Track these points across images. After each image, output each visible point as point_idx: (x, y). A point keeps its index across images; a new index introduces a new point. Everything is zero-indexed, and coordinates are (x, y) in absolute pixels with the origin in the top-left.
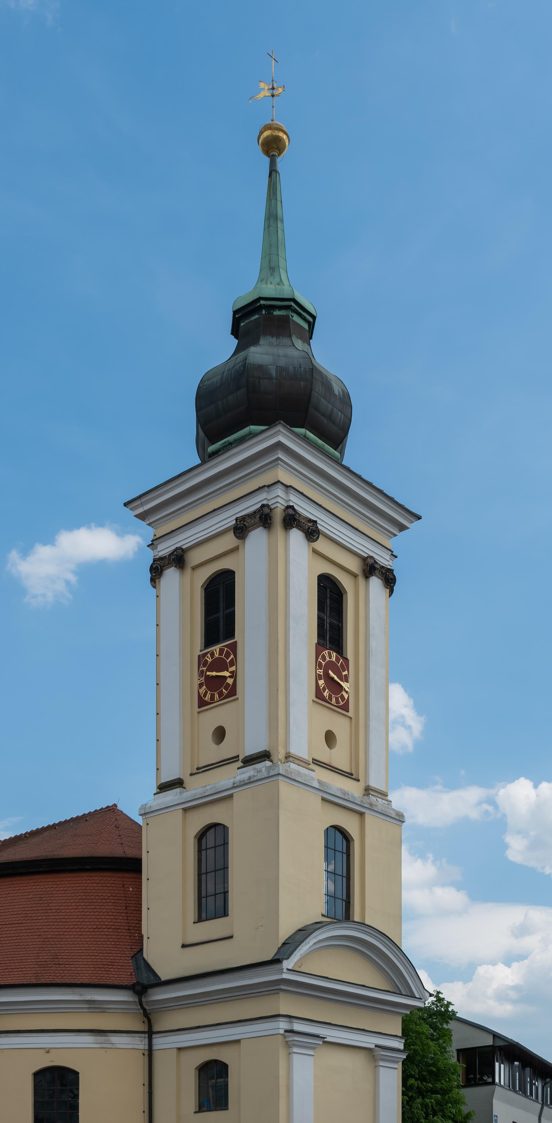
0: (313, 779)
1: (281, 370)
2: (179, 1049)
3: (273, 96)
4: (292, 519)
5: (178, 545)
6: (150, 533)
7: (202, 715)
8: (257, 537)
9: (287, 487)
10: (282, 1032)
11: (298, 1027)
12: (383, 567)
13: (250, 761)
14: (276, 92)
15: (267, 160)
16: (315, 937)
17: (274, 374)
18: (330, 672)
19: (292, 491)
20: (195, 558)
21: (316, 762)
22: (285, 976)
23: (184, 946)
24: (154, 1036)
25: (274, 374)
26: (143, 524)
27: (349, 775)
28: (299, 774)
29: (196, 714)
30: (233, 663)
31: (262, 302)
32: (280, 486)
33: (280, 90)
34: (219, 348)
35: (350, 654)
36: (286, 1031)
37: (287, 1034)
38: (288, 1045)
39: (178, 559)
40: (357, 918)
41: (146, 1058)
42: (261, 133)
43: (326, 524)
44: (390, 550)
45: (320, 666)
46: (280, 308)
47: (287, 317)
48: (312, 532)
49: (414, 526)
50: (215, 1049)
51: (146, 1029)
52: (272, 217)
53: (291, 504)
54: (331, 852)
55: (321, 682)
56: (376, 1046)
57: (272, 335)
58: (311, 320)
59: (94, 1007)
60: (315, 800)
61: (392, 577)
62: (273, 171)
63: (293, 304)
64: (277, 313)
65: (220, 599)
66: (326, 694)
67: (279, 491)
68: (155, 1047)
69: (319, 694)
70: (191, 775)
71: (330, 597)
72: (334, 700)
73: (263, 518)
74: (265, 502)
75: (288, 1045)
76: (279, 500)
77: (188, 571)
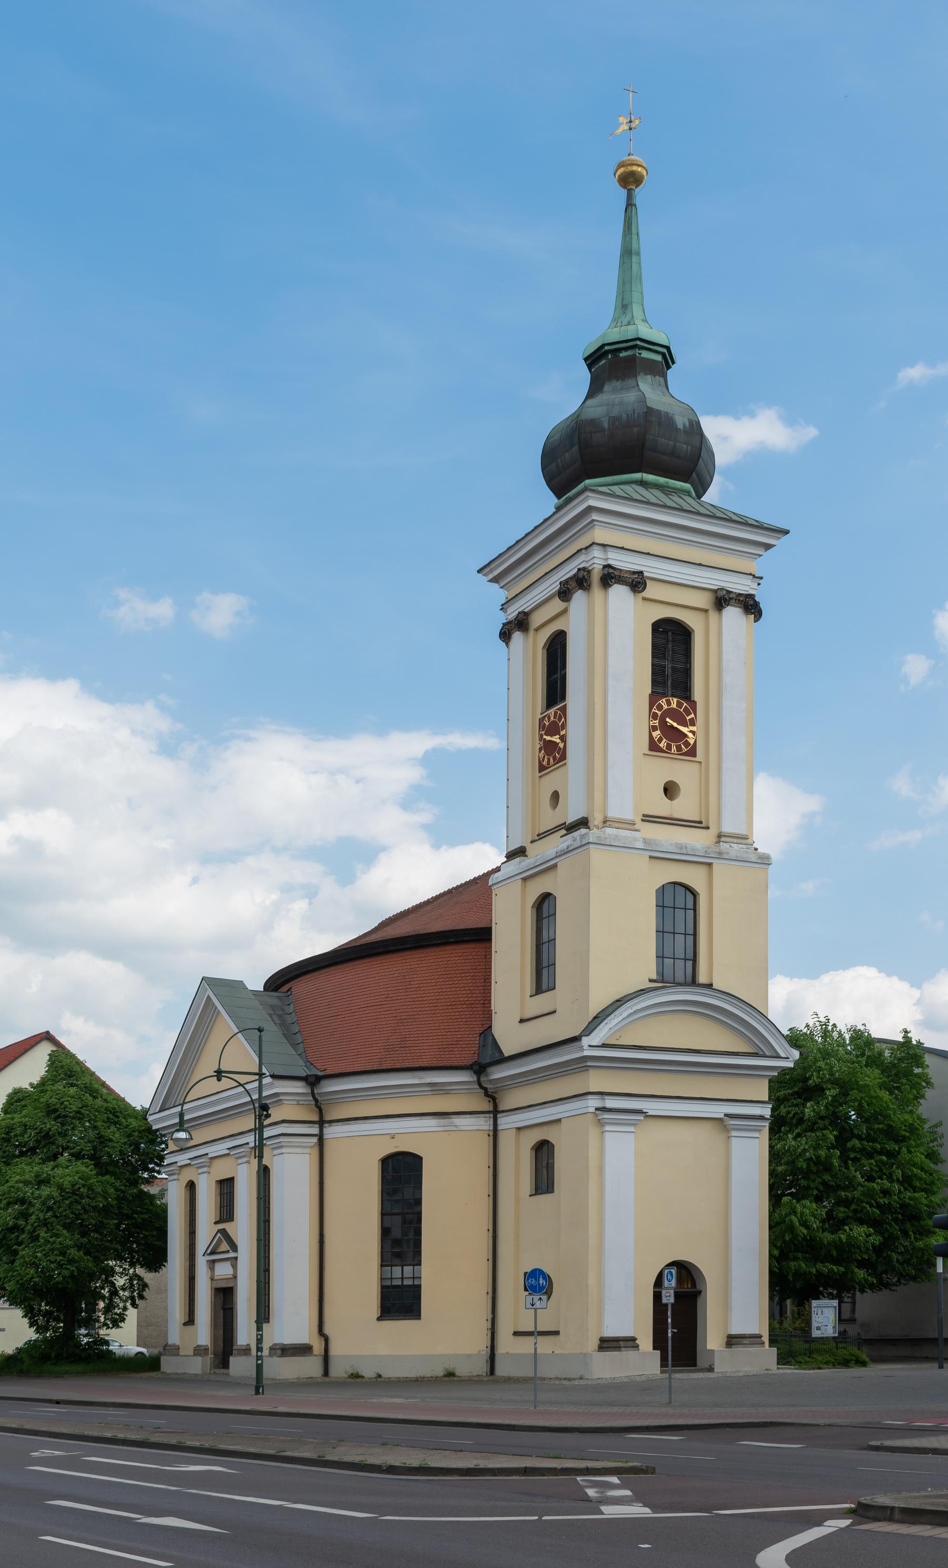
0: (636, 840)
1: (614, 420)
2: (519, 1129)
3: (630, 129)
4: (610, 577)
5: (520, 610)
6: (499, 594)
7: (543, 779)
8: (579, 597)
9: (604, 546)
10: (592, 1110)
11: (611, 1103)
12: (740, 595)
13: (571, 828)
14: (633, 125)
15: (624, 192)
16: (631, 1007)
17: (606, 425)
18: (668, 720)
19: (609, 549)
20: (537, 619)
21: (648, 818)
22: (586, 1053)
23: (522, 1021)
24: (499, 1116)
25: (606, 425)
26: (496, 585)
27: (697, 824)
28: (617, 837)
29: (537, 779)
30: (564, 726)
31: (607, 348)
32: (595, 547)
33: (637, 122)
34: (564, 394)
35: (698, 693)
36: (597, 1109)
37: (598, 1112)
38: (601, 1123)
39: (521, 623)
40: (702, 978)
41: (491, 1138)
42: (616, 171)
43: (650, 568)
44: (750, 574)
45: (655, 716)
46: (626, 349)
47: (634, 355)
48: (637, 582)
49: (780, 543)
50: (545, 1128)
51: (491, 1109)
52: (628, 253)
53: (610, 562)
54: (669, 912)
55: (656, 734)
56: (726, 1115)
57: (617, 379)
58: (665, 350)
59: (436, 1088)
60: (642, 860)
61: (751, 602)
62: (630, 204)
63: (638, 343)
64: (623, 354)
65: (556, 651)
66: (663, 745)
67: (596, 552)
68: (500, 1128)
69: (653, 746)
70: (532, 842)
71: (672, 649)
72: (674, 749)
73: (581, 581)
74: (581, 566)
75: (601, 1123)
76: (596, 561)
77: (531, 632)
